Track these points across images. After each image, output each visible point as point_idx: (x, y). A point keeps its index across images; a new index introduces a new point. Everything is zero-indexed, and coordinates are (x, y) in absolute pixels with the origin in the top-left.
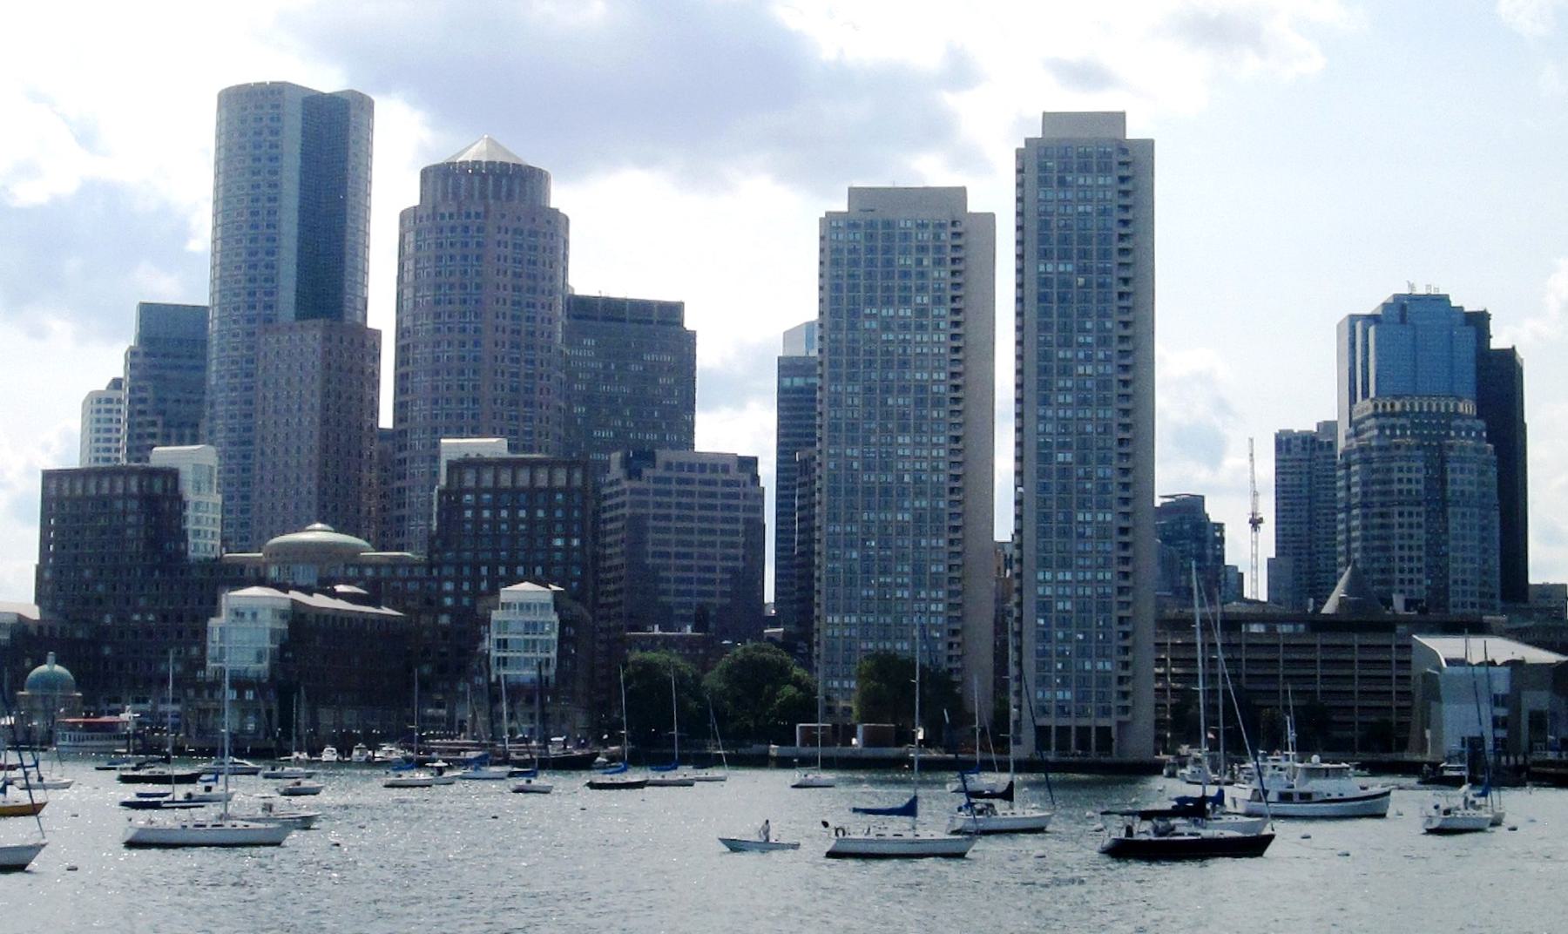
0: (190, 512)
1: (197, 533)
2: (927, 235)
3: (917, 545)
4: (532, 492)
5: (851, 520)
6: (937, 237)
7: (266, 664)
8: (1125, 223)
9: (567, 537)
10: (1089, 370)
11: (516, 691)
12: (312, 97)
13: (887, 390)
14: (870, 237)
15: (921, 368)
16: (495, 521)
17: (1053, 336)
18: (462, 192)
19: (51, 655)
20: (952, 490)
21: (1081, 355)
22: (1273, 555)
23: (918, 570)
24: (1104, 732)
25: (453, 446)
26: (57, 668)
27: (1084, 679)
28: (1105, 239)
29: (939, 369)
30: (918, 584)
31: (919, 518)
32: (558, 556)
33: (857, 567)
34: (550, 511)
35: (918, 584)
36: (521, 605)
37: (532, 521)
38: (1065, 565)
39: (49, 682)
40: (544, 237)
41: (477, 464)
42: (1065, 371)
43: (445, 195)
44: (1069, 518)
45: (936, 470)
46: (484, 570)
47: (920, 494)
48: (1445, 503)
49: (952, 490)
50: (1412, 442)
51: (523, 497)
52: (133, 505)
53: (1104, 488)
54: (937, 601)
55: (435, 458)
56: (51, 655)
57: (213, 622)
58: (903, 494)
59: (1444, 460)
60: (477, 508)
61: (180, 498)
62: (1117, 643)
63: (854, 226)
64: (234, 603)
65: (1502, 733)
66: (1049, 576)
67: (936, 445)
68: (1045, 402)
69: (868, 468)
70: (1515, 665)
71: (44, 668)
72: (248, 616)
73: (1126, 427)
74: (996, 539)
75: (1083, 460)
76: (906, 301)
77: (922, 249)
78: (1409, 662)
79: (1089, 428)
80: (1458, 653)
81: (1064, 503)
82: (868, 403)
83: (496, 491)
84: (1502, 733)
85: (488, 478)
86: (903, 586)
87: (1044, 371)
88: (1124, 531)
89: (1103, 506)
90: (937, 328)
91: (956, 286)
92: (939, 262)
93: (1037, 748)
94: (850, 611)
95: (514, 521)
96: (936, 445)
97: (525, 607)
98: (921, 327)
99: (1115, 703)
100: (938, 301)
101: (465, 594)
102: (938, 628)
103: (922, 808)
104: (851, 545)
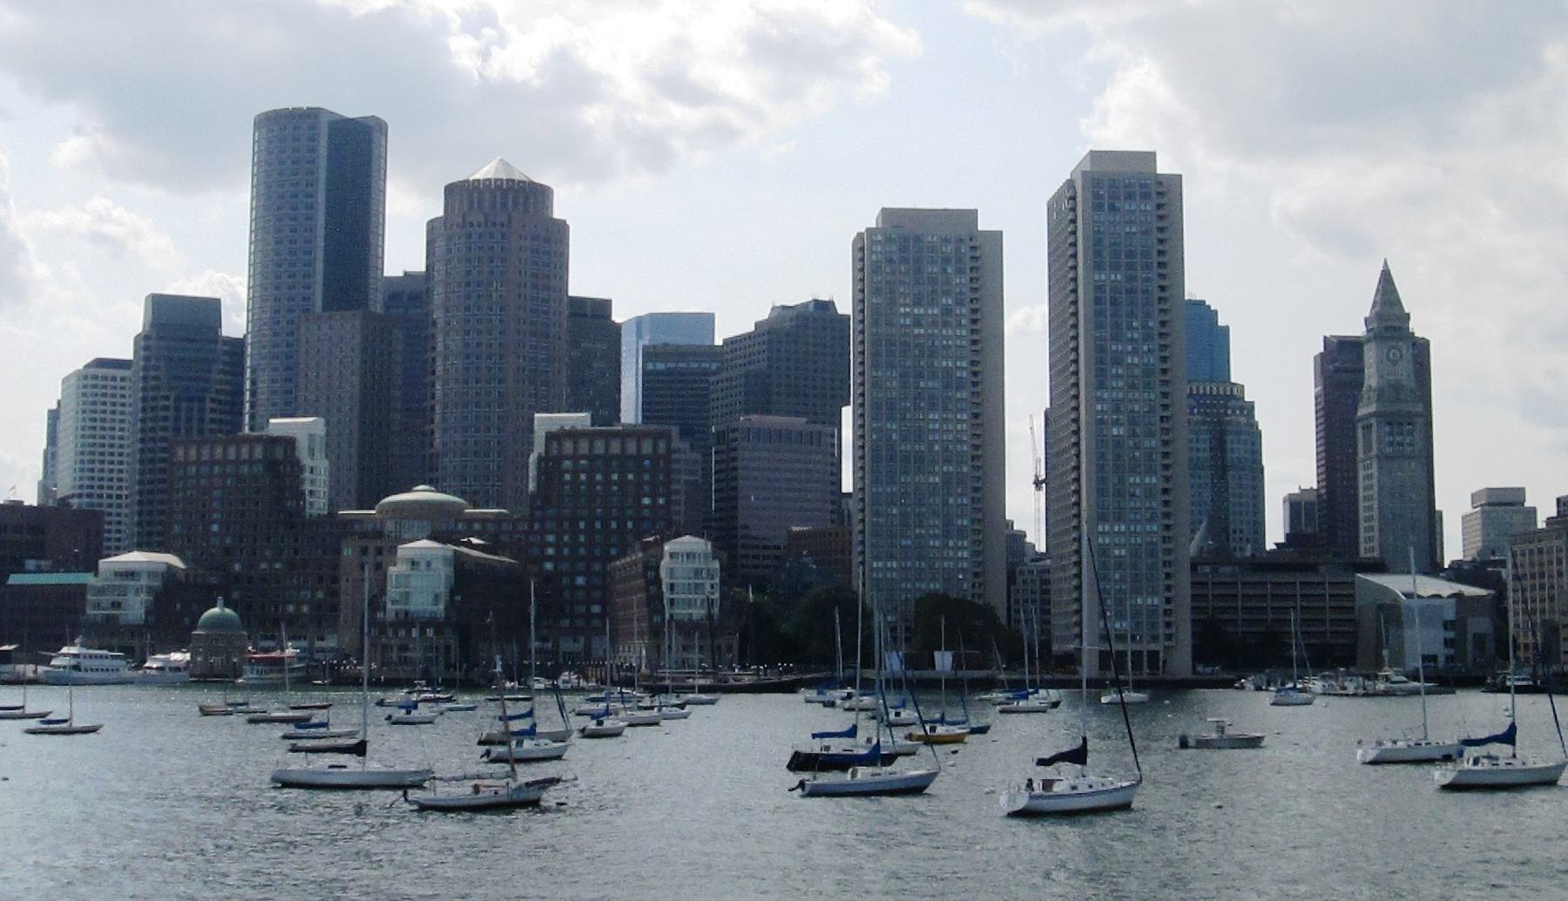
0: (307, 475)
1: (311, 492)
2: (949, 248)
3: (945, 503)
4: (623, 457)
5: (892, 482)
6: (958, 250)
7: (442, 606)
8: (1161, 241)
9: (654, 497)
10: (1136, 360)
11: (687, 629)
12: (337, 122)
13: (920, 376)
14: (903, 249)
15: (947, 357)
16: (591, 483)
17: (1107, 333)
18: (486, 204)
19: (220, 600)
20: (973, 458)
21: (1130, 348)
22: (1554, 514)
23: (948, 523)
24: (1153, 655)
25: (545, 421)
26: (227, 611)
27: (1137, 613)
28: (1146, 254)
29: (962, 358)
30: (947, 535)
31: (947, 479)
32: (646, 513)
33: (897, 521)
34: (638, 475)
35: (947, 535)
36: (688, 555)
37: (622, 483)
38: (1119, 518)
39: (217, 623)
40: (550, 242)
41: (574, 435)
42: (1118, 361)
43: (471, 208)
44: (1121, 481)
45: (960, 441)
46: (582, 525)
47: (947, 461)
48: (1224, 468)
49: (973, 458)
50: (1199, 418)
51: (599, 462)
52: (258, 469)
53: (1149, 455)
54: (963, 548)
55: (530, 430)
56: (220, 600)
57: (392, 570)
58: (934, 462)
59: (1223, 433)
60: (575, 472)
61: (298, 462)
62: (1162, 582)
63: (889, 240)
64: (410, 554)
65: (1451, 651)
66: (1107, 528)
67: (960, 421)
68: (1101, 386)
69: (904, 439)
70: (1458, 596)
71: (216, 610)
72: (423, 565)
73: (1166, 407)
74: (571, 293)
75: (1134, 434)
76: (933, 303)
77: (946, 260)
78: (1352, 596)
79: (1137, 408)
80: (1409, 588)
81: (1117, 468)
82: (904, 386)
83: (592, 458)
84: (1451, 651)
85: (584, 447)
86: (935, 537)
87: (1100, 361)
88: (1165, 491)
89: (1150, 471)
90: (959, 325)
91: (975, 290)
92: (960, 271)
93: (1101, 668)
94: (891, 557)
95: (607, 483)
96: (960, 421)
97: (690, 556)
98: (946, 324)
99: (1161, 631)
100: (960, 303)
101: (566, 545)
102: (963, 570)
103: (536, 713)
104: (891, 503)
